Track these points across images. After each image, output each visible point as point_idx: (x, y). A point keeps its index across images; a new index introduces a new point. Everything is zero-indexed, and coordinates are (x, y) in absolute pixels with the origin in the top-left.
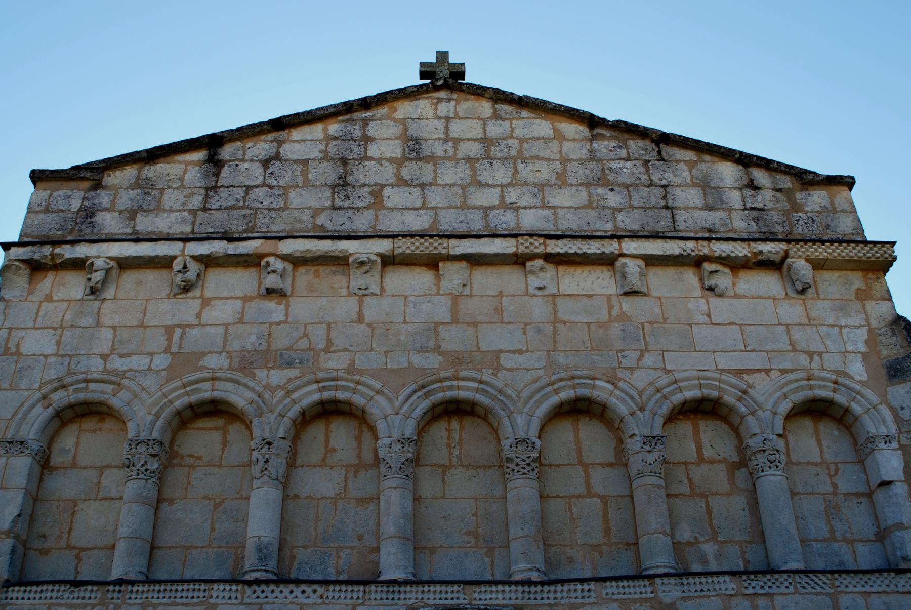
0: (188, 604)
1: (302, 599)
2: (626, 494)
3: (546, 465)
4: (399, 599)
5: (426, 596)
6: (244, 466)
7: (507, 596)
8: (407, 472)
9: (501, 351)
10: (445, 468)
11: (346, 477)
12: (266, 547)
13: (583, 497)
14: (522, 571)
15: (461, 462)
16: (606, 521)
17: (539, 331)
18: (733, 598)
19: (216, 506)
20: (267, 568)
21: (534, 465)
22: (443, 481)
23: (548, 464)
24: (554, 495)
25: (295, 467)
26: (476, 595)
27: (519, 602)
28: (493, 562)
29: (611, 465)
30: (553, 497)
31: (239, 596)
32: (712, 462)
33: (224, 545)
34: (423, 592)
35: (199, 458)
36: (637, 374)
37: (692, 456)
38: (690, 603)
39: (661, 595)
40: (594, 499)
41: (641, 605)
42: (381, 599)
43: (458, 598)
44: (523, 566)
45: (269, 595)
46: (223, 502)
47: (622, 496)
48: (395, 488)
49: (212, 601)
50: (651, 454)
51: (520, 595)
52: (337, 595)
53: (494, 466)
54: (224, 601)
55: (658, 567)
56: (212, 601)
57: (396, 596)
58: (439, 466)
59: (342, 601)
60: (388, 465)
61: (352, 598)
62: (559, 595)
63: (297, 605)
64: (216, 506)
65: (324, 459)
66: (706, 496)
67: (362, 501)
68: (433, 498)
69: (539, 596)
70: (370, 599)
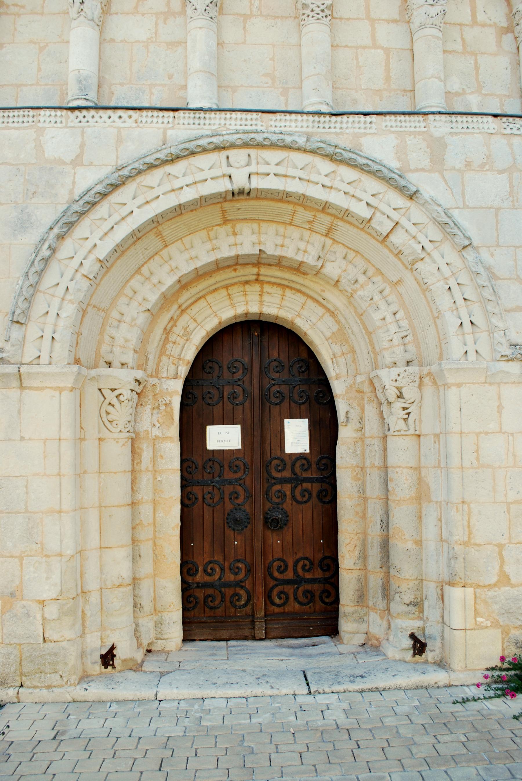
0: (20, 127)
1: (119, 123)
2: (407, 48)
3: (337, 18)
4: (204, 124)
5: (228, 122)
6: (64, 14)
7: (299, 124)
8: (211, 15)
10: (246, 17)
11: (156, 24)
12: (85, 80)
13: (369, 48)
14: (313, 104)
15: (261, 12)
16: (388, 70)
18: (493, 136)
19: (41, 49)
20: (87, 98)
21: (328, 12)
22: (244, 28)
23: (339, 17)
24: (344, 45)
25: (110, 14)
26: (273, 123)
27: (310, 130)
28: (287, 100)
29: (395, 21)
30: (342, 46)
31: (64, 121)
32: (484, 25)
33: (50, 83)
34: (225, 119)
35: (23, 7)
37: (467, 18)
38: (456, 138)
39: (432, 129)
40: (379, 51)
41: (415, 137)
42: (189, 124)
43: (256, 125)
44: (314, 99)
45: (90, 120)
46: (47, 45)
47: (403, 49)
48: (200, 28)
49: (40, 125)
50: (434, 8)
51: (310, 124)
52: (149, 120)
53: (290, 17)
54: (50, 125)
55: (431, 106)
56: (40, 125)
57: (202, 122)
58: (241, 15)
59: (153, 125)
60: (194, 7)
61: (163, 123)
62: (344, 125)
63: (115, 128)
64: (41, 49)
65: (136, 8)
66: (476, 55)
67: (172, 45)
68: (235, 44)
69: (327, 126)
70: (179, 124)
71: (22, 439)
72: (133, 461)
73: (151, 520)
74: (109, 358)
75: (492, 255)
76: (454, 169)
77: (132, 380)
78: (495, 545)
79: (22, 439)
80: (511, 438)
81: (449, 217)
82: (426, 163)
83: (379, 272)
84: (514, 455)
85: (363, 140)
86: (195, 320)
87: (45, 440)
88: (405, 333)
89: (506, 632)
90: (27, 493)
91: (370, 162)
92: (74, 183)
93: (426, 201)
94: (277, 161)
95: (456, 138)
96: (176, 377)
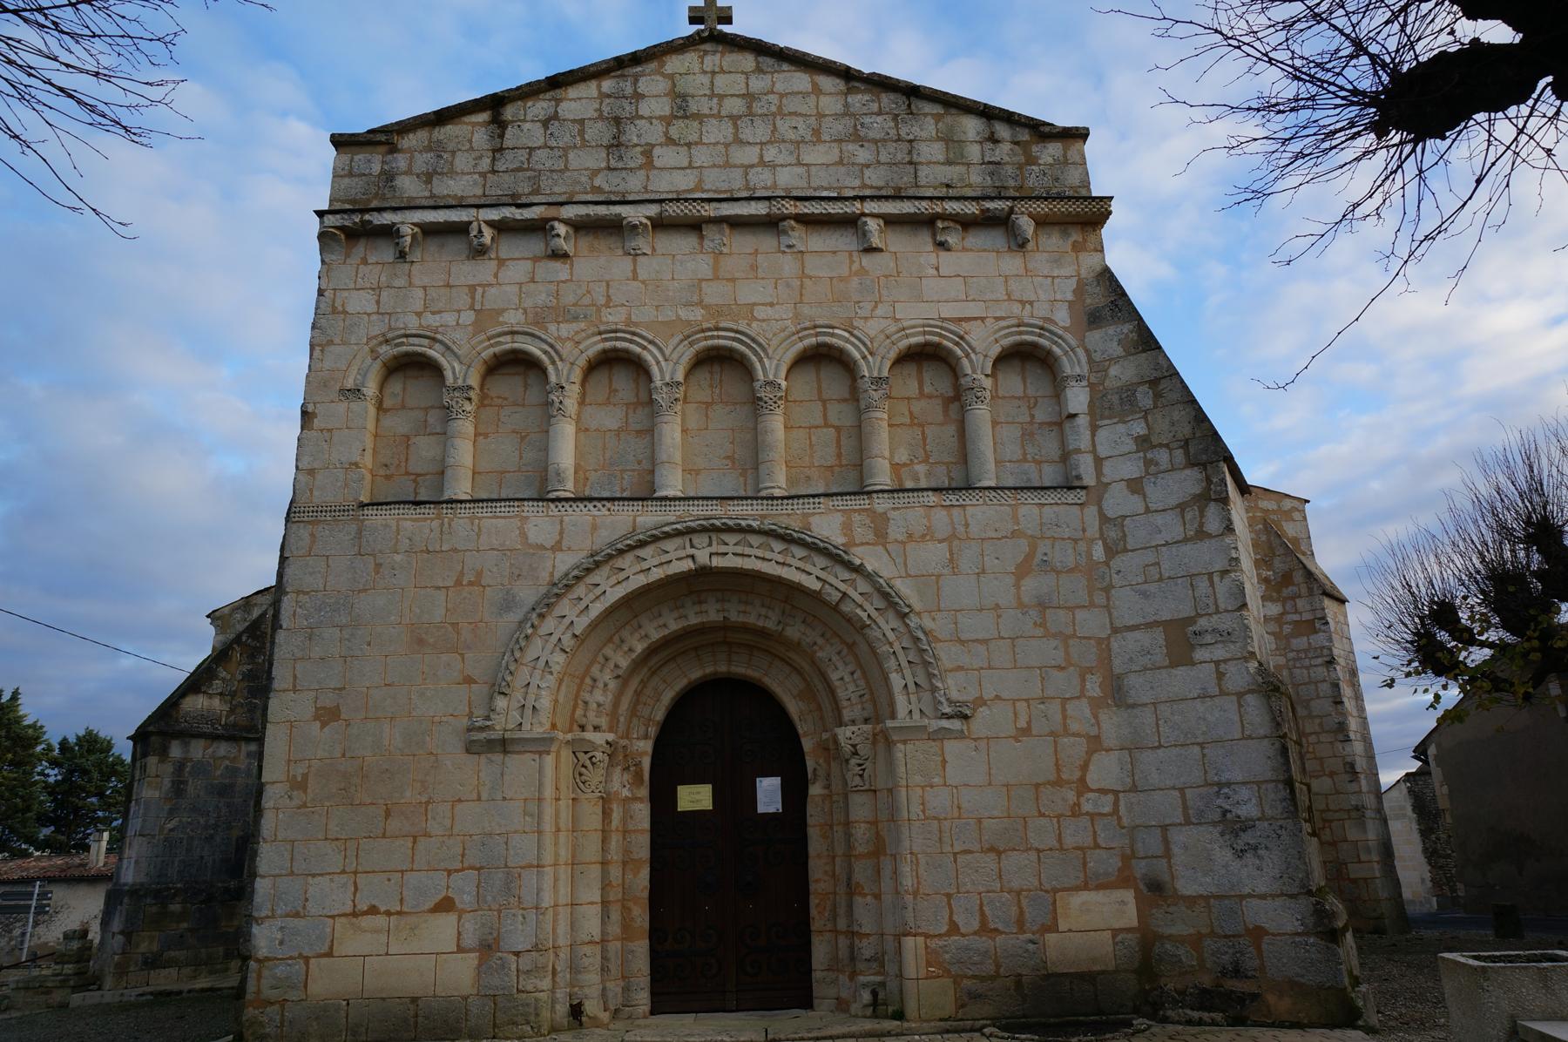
9: (755, 304)
11: (627, 414)
17: (788, 285)
28: (746, 480)
29: (845, 400)
36: (871, 323)
45: (569, 509)
64: (523, 438)
66: (923, 426)
71: (504, 799)
72: (603, 821)
73: (620, 881)
74: (584, 721)
75: (934, 619)
76: (896, 541)
77: (603, 743)
78: (944, 895)
79: (504, 799)
80: (955, 791)
81: (891, 588)
82: (871, 537)
83: (836, 634)
84: (959, 808)
85: (811, 519)
86: (665, 681)
87: (525, 800)
88: (862, 692)
89: (957, 980)
90: (507, 849)
91: (817, 541)
92: (554, 566)
93: (869, 573)
94: (735, 542)
95: (897, 512)
96: (646, 737)
